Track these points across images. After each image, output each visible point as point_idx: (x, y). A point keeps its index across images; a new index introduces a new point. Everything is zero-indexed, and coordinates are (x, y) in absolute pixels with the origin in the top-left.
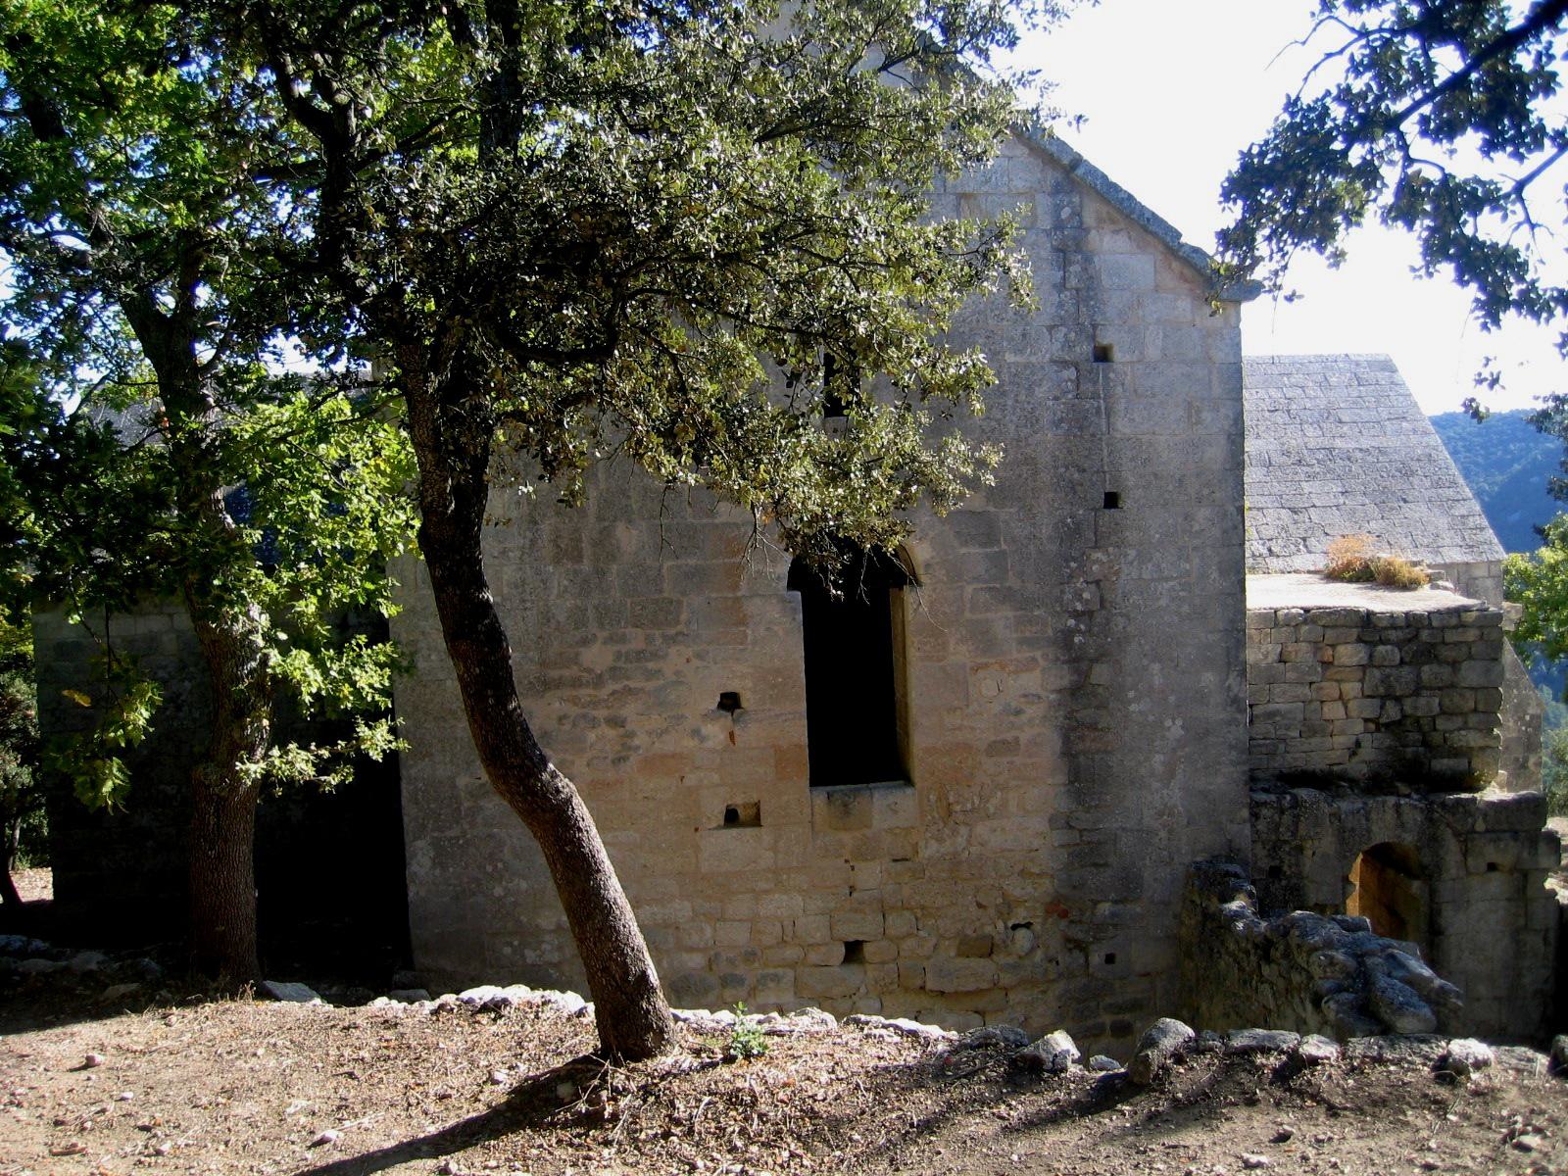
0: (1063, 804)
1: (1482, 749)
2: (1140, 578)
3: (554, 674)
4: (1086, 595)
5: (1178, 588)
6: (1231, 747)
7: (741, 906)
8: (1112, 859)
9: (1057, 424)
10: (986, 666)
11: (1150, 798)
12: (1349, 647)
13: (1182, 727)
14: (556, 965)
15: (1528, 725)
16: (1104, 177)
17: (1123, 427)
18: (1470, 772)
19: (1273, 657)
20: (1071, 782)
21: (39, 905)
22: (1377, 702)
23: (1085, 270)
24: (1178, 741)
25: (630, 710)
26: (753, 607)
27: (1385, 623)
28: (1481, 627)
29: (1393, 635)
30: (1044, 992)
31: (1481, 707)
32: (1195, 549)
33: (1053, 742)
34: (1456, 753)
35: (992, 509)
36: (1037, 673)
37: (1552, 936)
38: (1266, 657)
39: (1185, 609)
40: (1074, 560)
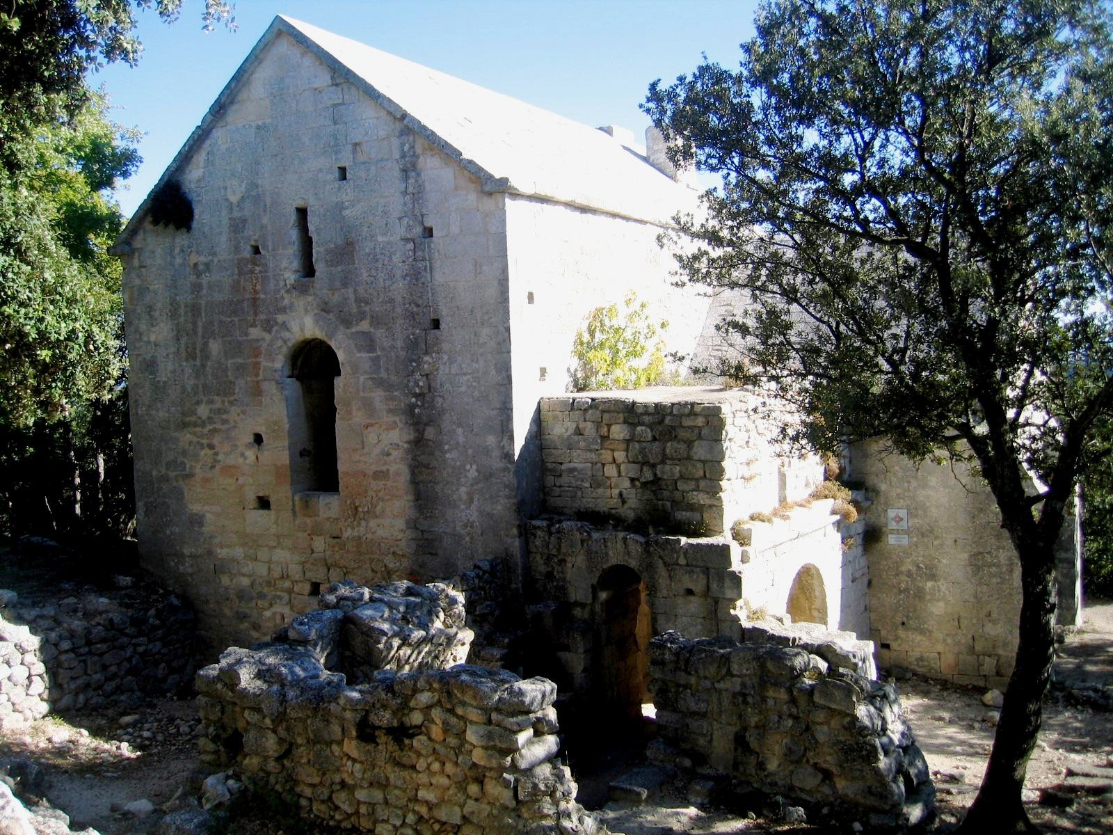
0: (411, 513)
1: (711, 506)
3: (188, 419)
4: (421, 383)
6: (506, 486)
7: (263, 554)
8: (440, 552)
9: (404, 277)
10: (372, 425)
13: (477, 471)
14: (191, 575)
16: (419, 122)
17: (439, 278)
18: (702, 522)
19: (571, 431)
20: (417, 500)
21: (648, 718)
22: (637, 466)
23: (417, 181)
25: (216, 440)
26: (266, 386)
27: (640, 410)
28: (706, 416)
29: (647, 419)
32: (481, 355)
34: (691, 508)
35: (372, 330)
36: (397, 430)
38: (567, 430)
39: (476, 394)
40: (414, 361)
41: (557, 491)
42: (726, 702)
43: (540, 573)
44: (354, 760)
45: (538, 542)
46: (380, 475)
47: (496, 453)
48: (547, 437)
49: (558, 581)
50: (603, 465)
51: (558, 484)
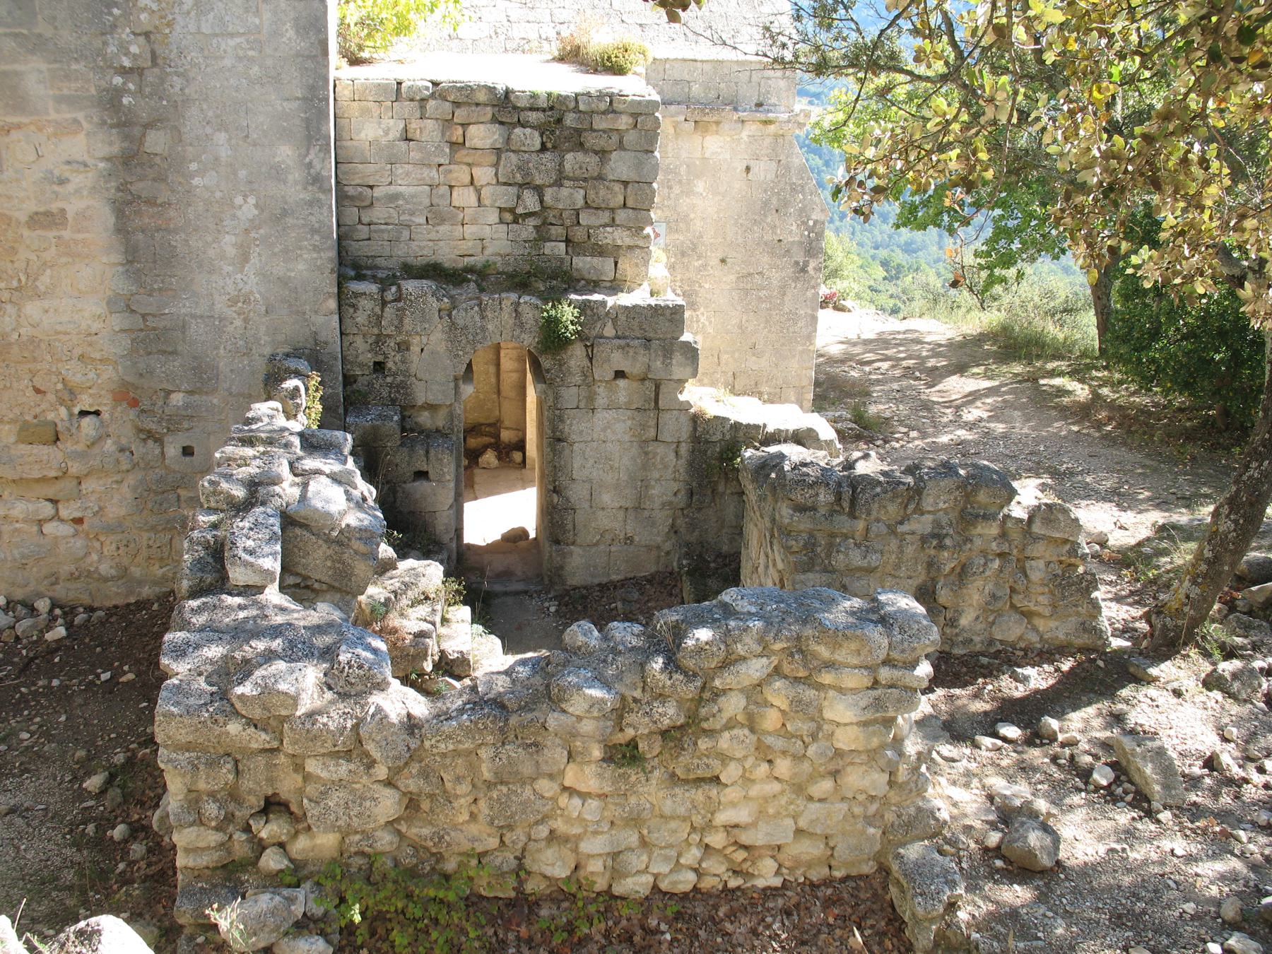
0: (123, 286)
1: (630, 248)
2: (199, 32)
4: (134, 49)
5: (245, 45)
11: (221, 283)
12: (482, 127)
13: (256, 206)
15: (811, 230)
20: (130, 262)
24: (252, 221)
28: (635, 115)
29: (533, 117)
30: (119, 482)
31: (630, 203)
33: (107, 217)
34: (600, 251)
37: (684, 449)
41: (363, 231)
42: (910, 550)
43: (361, 365)
44: (584, 796)
45: (361, 318)
46: (46, 219)
47: (296, 175)
48: (349, 143)
49: (395, 375)
50: (451, 187)
51: (365, 220)
